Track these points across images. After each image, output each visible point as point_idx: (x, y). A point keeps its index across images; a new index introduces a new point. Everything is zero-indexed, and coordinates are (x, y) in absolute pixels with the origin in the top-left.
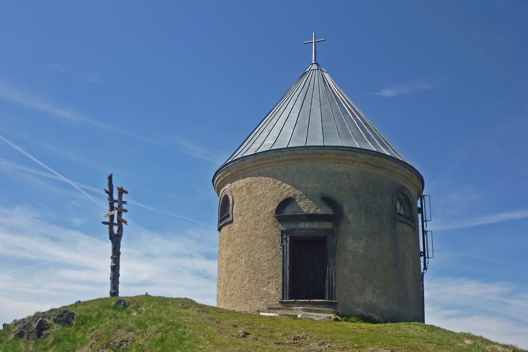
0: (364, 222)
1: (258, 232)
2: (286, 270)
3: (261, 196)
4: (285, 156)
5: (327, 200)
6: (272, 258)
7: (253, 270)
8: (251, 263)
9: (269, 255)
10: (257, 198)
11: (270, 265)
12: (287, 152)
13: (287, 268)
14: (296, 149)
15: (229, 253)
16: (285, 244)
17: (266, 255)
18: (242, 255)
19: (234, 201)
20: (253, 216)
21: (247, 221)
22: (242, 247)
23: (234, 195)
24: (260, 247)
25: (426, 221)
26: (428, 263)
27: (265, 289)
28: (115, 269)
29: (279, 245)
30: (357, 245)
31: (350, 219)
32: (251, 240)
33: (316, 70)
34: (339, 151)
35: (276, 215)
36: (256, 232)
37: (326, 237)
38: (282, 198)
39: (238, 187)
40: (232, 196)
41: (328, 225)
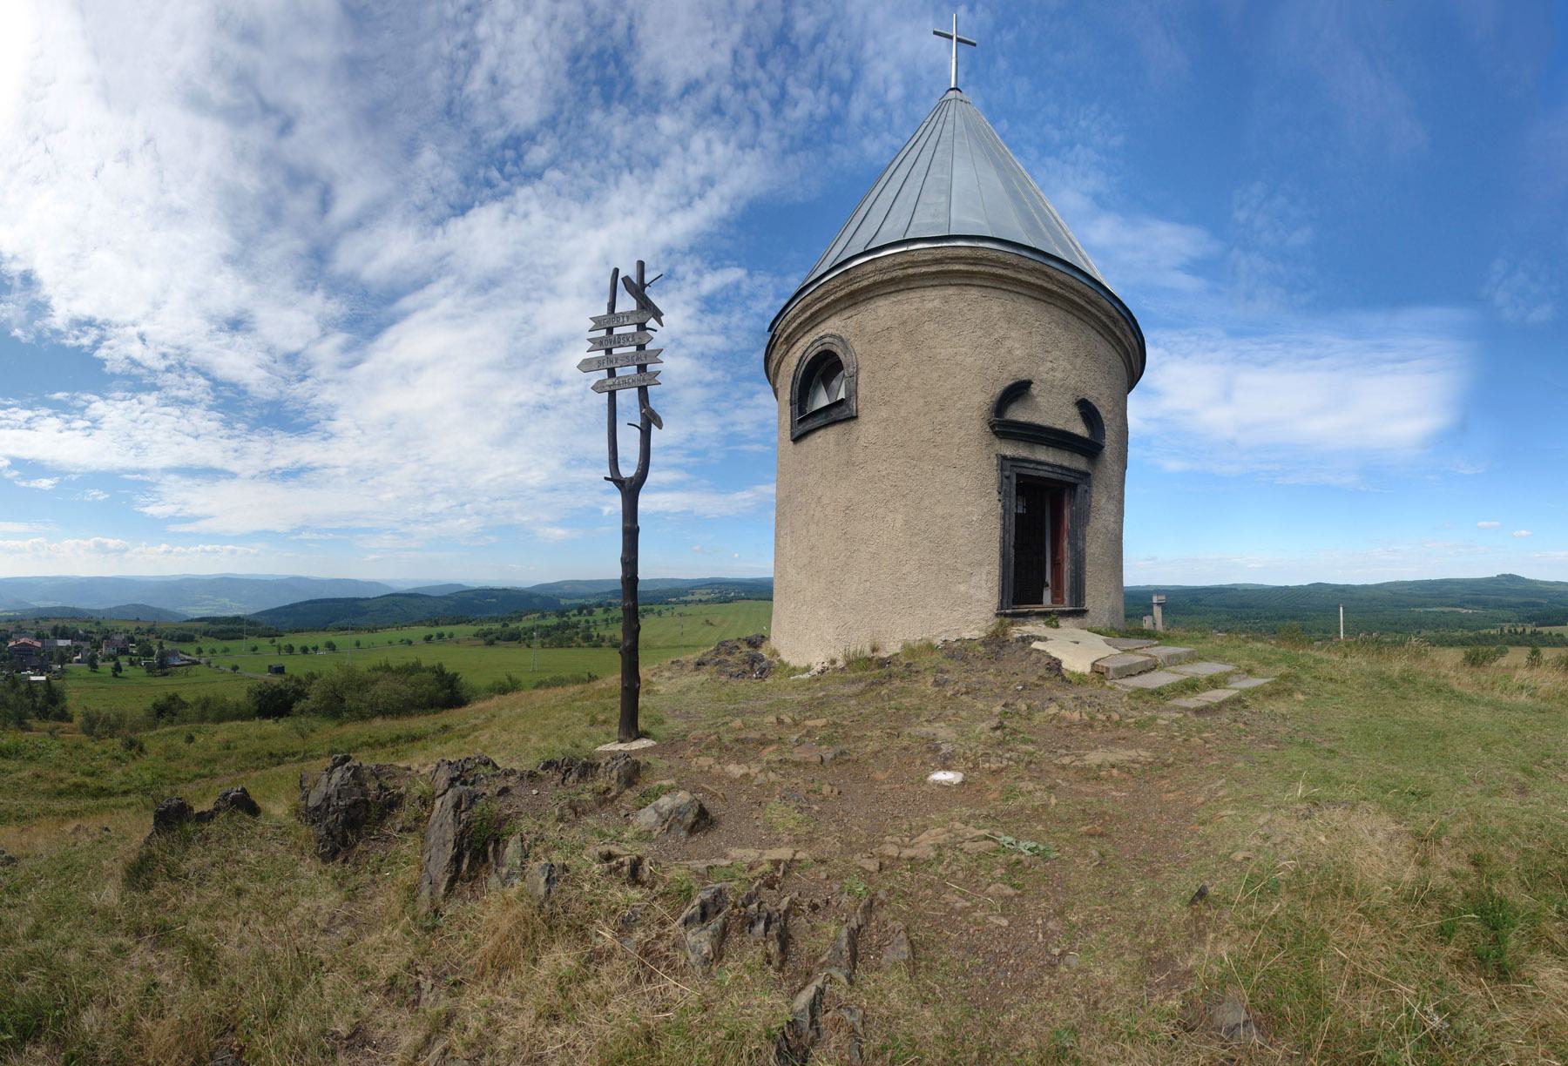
1: (941, 453)
9: (970, 513)
20: (926, 409)
27: (962, 588)
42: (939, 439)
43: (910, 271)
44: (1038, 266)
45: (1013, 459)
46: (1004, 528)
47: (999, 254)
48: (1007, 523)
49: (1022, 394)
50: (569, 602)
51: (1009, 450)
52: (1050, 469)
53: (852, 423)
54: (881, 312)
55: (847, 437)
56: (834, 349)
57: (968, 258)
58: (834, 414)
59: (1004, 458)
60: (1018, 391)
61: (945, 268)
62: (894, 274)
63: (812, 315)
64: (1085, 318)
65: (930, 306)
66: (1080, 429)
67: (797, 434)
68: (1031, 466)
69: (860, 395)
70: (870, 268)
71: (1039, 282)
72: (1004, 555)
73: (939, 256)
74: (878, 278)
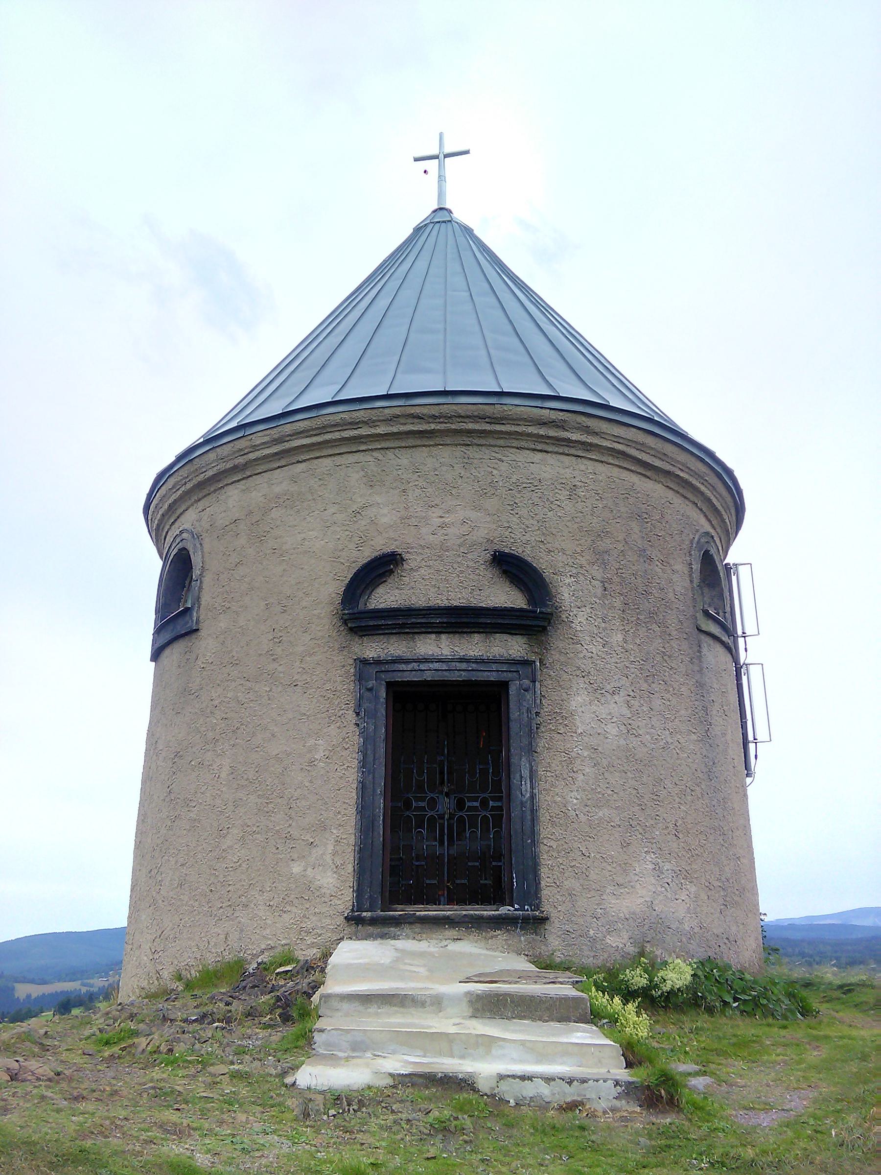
0: (620, 637)
4: (379, 423)
12: (387, 411)
18: (223, 744)
25: (744, 637)
26: (756, 756)
27: (296, 868)
30: (603, 711)
36: (276, 665)
37: (504, 686)
39: (221, 521)
43: (252, 456)
44: (397, 411)
45: (378, 662)
46: (364, 764)
48: (370, 758)
49: (391, 572)
50: (36, 991)
53: (194, 636)
54: (231, 503)
57: (308, 431)
59: (363, 662)
61: (287, 445)
62: (237, 461)
64: (501, 442)
65: (277, 489)
68: (410, 667)
69: (203, 602)
70: (212, 456)
72: (364, 809)
73: (276, 436)
74: (222, 466)
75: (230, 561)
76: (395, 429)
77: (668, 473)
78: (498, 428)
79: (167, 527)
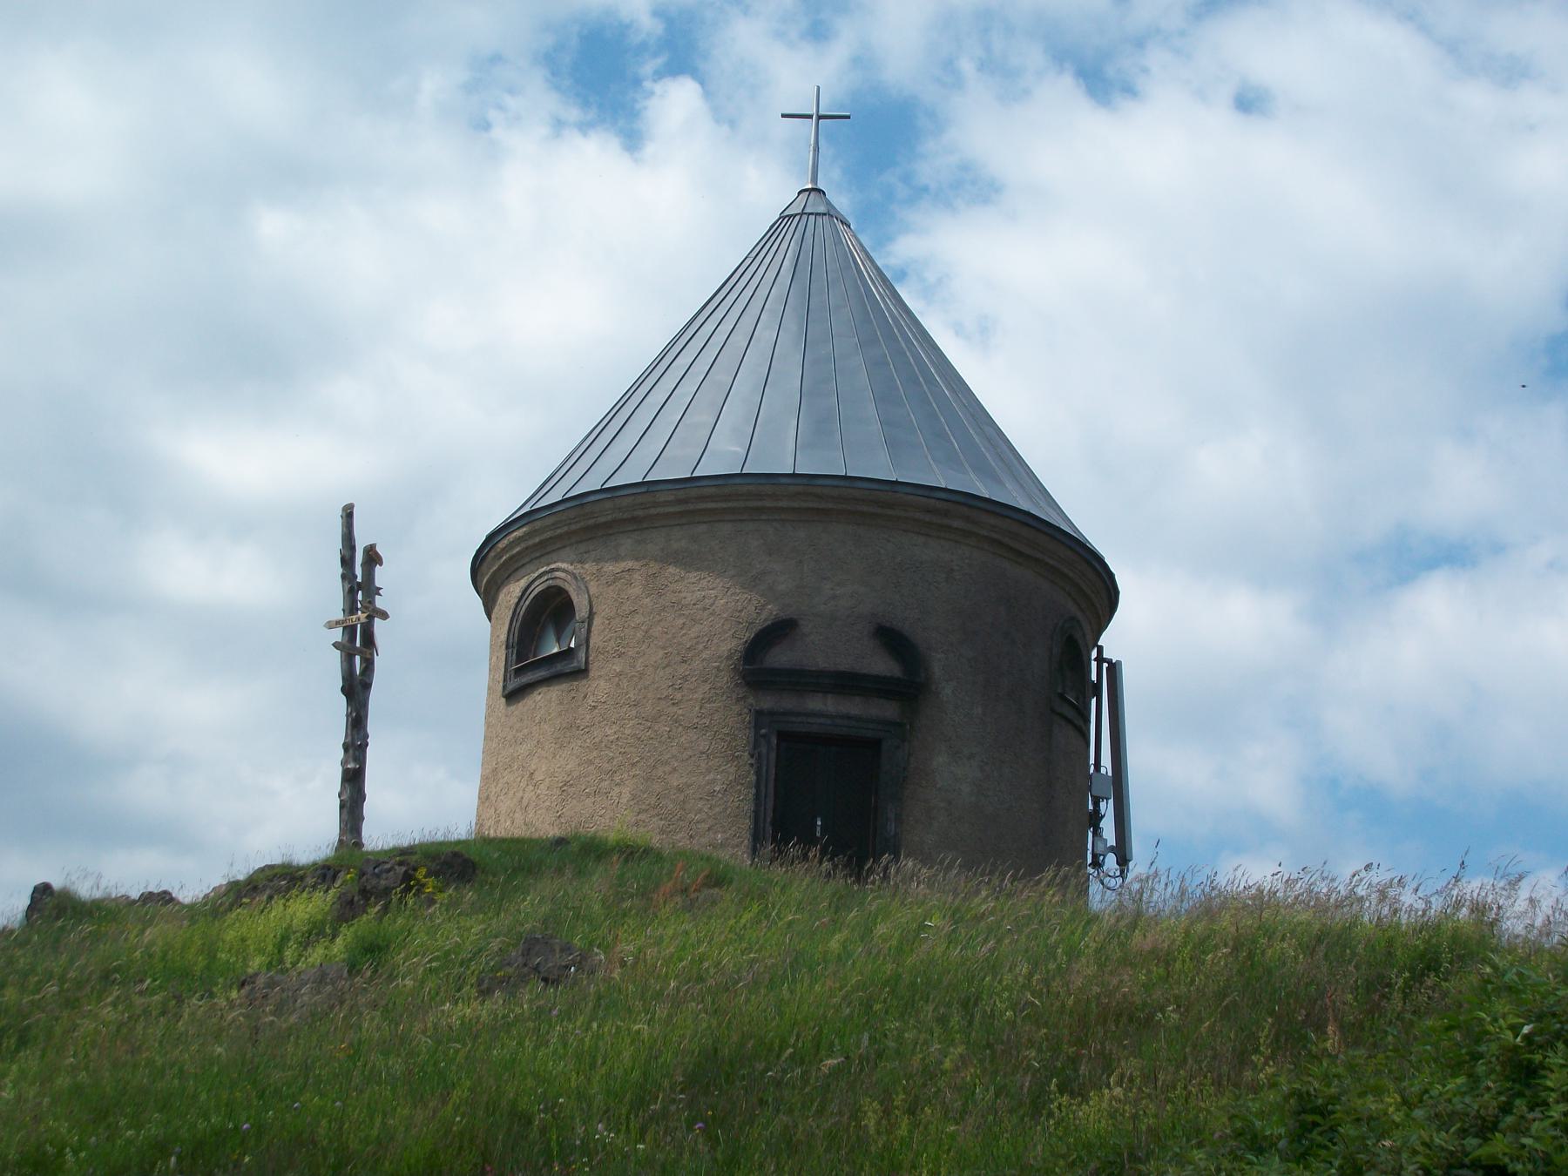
1: (680, 712)
2: (764, 827)
3: (694, 604)
5: (891, 639)
6: (726, 790)
7: (661, 819)
8: (653, 800)
9: (714, 781)
10: (680, 609)
11: (717, 809)
12: (791, 488)
13: (769, 820)
14: (820, 482)
15: (569, 766)
16: (764, 751)
17: (707, 778)
19: (594, 610)
20: (666, 661)
21: (641, 675)
22: (623, 750)
23: (593, 590)
24: (685, 756)
28: (353, 779)
29: (746, 754)
31: (945, 699)
32: (656, 731)
33: (812, 218)
34: (933, 501)
35: (744, 664)
36: (675, 709)
37: (876, 744)
38: (763, 617)
40: (589, 596)
41: (888, 710)
42: (678, 696)
43: (653, 511)
45: (771, 713)
47: (750, 487)
51: (767, 702)
52: (829, 722)
55: (573, 694)
56: (567, 587)
58: (559, 667)
60: (777, 632)
61: (691, 507)
62: (636, 513)
63: (541, 542)
66: (882, 665)
67: (511, 687)
70: (608, 505)
71: (811, 505)
75: (623, 608)
76: (796, 505)
77: (1037, 560)
78: (889, 512)
79: (527, 560)
